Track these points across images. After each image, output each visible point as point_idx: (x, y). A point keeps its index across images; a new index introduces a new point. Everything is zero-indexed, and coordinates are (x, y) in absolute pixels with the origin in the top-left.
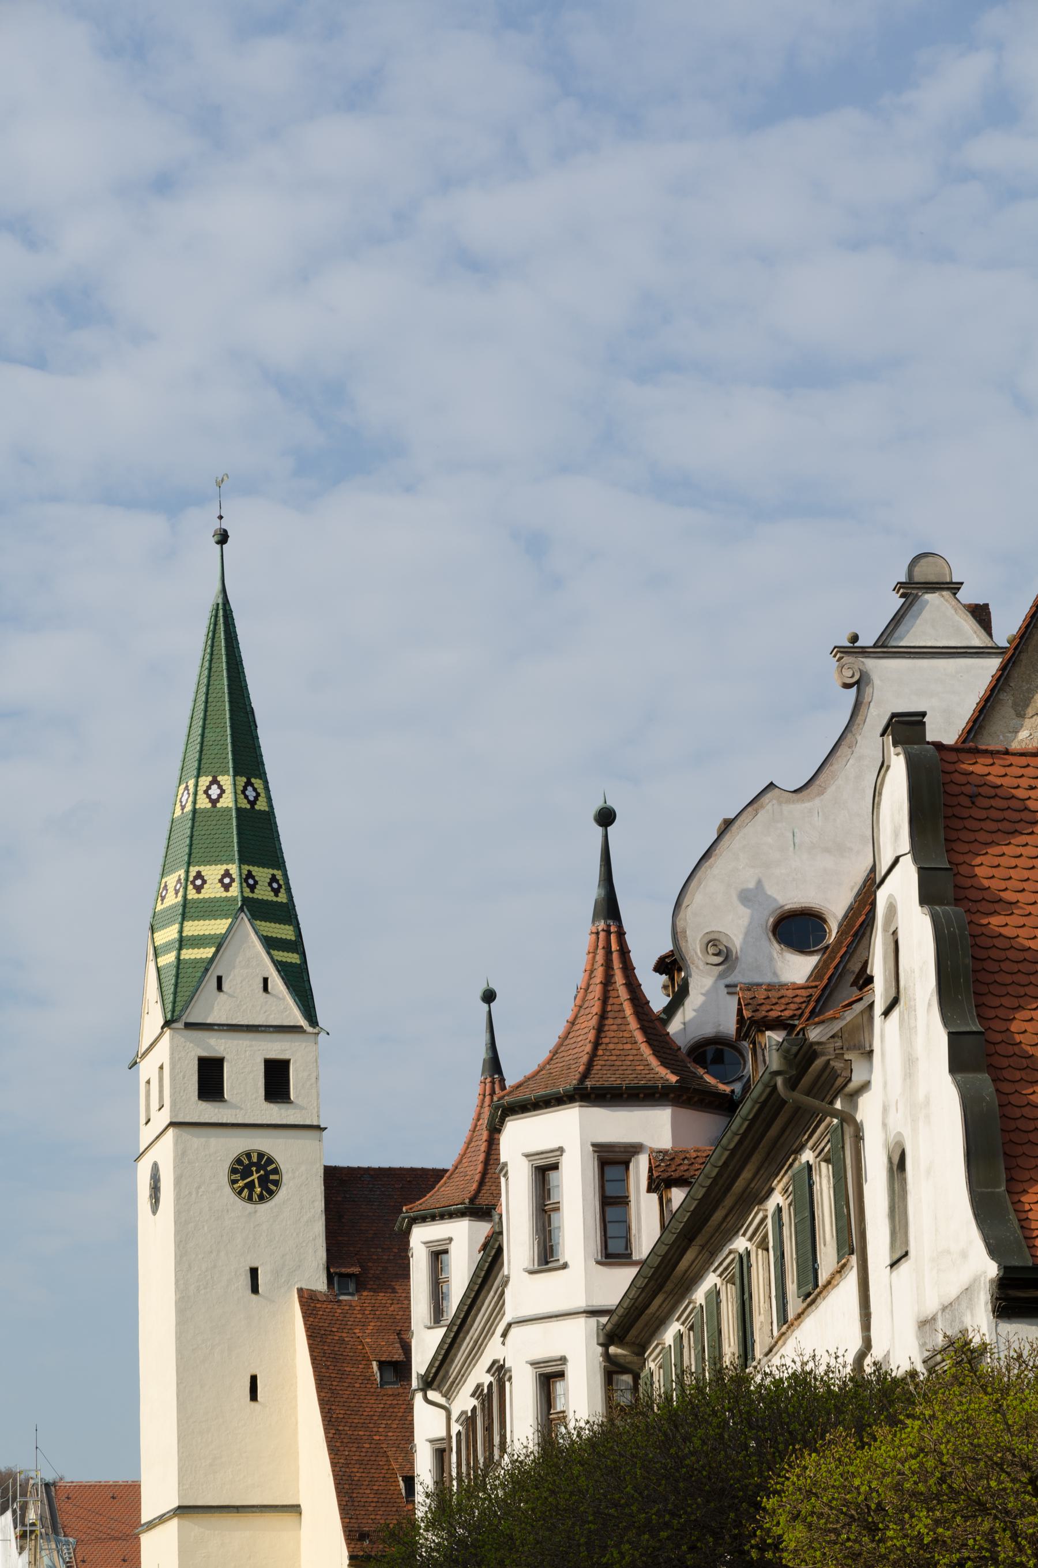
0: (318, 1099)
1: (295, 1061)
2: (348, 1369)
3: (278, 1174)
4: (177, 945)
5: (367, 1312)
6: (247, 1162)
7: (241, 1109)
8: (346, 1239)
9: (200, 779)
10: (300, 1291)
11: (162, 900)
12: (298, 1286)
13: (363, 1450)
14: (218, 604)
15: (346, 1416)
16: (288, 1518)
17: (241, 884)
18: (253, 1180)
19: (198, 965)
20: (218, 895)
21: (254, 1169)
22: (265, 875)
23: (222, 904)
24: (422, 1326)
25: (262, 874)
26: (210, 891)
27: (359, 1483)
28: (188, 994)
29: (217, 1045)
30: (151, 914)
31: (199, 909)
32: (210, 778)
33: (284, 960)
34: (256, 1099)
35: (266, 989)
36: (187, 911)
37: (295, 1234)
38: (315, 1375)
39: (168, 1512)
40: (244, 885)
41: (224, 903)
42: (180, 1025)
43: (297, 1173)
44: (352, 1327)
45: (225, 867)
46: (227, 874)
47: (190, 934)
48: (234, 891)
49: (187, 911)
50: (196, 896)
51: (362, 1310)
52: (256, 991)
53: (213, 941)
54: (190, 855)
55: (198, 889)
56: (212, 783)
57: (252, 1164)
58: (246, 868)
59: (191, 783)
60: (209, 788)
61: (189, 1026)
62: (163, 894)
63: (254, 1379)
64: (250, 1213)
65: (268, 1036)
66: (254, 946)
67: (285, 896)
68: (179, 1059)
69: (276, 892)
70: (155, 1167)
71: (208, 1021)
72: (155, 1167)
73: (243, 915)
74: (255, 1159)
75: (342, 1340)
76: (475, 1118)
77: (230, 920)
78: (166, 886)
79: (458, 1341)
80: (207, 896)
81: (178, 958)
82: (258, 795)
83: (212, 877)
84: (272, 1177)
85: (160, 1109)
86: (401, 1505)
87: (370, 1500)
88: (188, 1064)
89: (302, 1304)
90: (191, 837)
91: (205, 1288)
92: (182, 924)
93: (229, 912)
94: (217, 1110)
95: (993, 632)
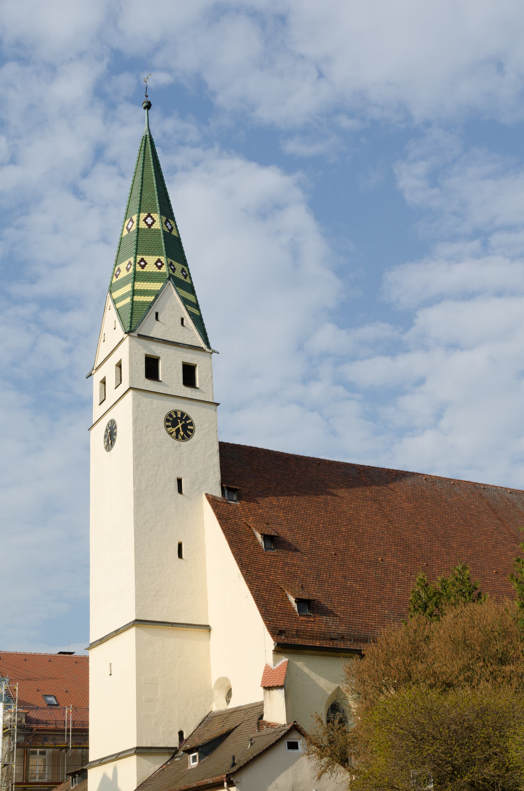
0: (212, 389)
1: (199, 367)
4: (131, 293)
6: (175, 417)
7: (170, 387)
9: (140, 214)
10: (207, 495)
14: (146, 135)
16: (202, 633)
18: (179, 428)
19: (145, 304)
20: (155, 271)
21: (179, 421)
23: (157, 275)
25: (178, 266)
26: (149, 268)
29: (156, 350)
30: (109, 284)
31: (143, 277)
32: (147, 214)
34: (178, 383)
36: (136, 277)
37: (203, 462)
38: (227, 539)
41: (158, 275)
42: (135, 334)
43: (203, 427)
46: (159, 261)
47: (139, 288)
48: (164, 269)
50: (141, 270)
52: (178, 324)
54: (137, 249)
55: (143, 267)
57: (177, 418)
58: (170, 260)
59: (135, 218)
61: (140, 336)
62: (117, 274)
63: (180, 546)
64: (177, 446)
65: (185, 350)
66: (176, 300)
68: (134, 353)
71: (151, 335)
73: (169, 282)
74: (179, 416)
75: (236, 523)
77: (162, 284)
81: (132, 300)
83: (151, 262)
84: (189, 427)
90: (137, 241)
91: (151, 486)
92: (134, 283)
94: (156, 386)
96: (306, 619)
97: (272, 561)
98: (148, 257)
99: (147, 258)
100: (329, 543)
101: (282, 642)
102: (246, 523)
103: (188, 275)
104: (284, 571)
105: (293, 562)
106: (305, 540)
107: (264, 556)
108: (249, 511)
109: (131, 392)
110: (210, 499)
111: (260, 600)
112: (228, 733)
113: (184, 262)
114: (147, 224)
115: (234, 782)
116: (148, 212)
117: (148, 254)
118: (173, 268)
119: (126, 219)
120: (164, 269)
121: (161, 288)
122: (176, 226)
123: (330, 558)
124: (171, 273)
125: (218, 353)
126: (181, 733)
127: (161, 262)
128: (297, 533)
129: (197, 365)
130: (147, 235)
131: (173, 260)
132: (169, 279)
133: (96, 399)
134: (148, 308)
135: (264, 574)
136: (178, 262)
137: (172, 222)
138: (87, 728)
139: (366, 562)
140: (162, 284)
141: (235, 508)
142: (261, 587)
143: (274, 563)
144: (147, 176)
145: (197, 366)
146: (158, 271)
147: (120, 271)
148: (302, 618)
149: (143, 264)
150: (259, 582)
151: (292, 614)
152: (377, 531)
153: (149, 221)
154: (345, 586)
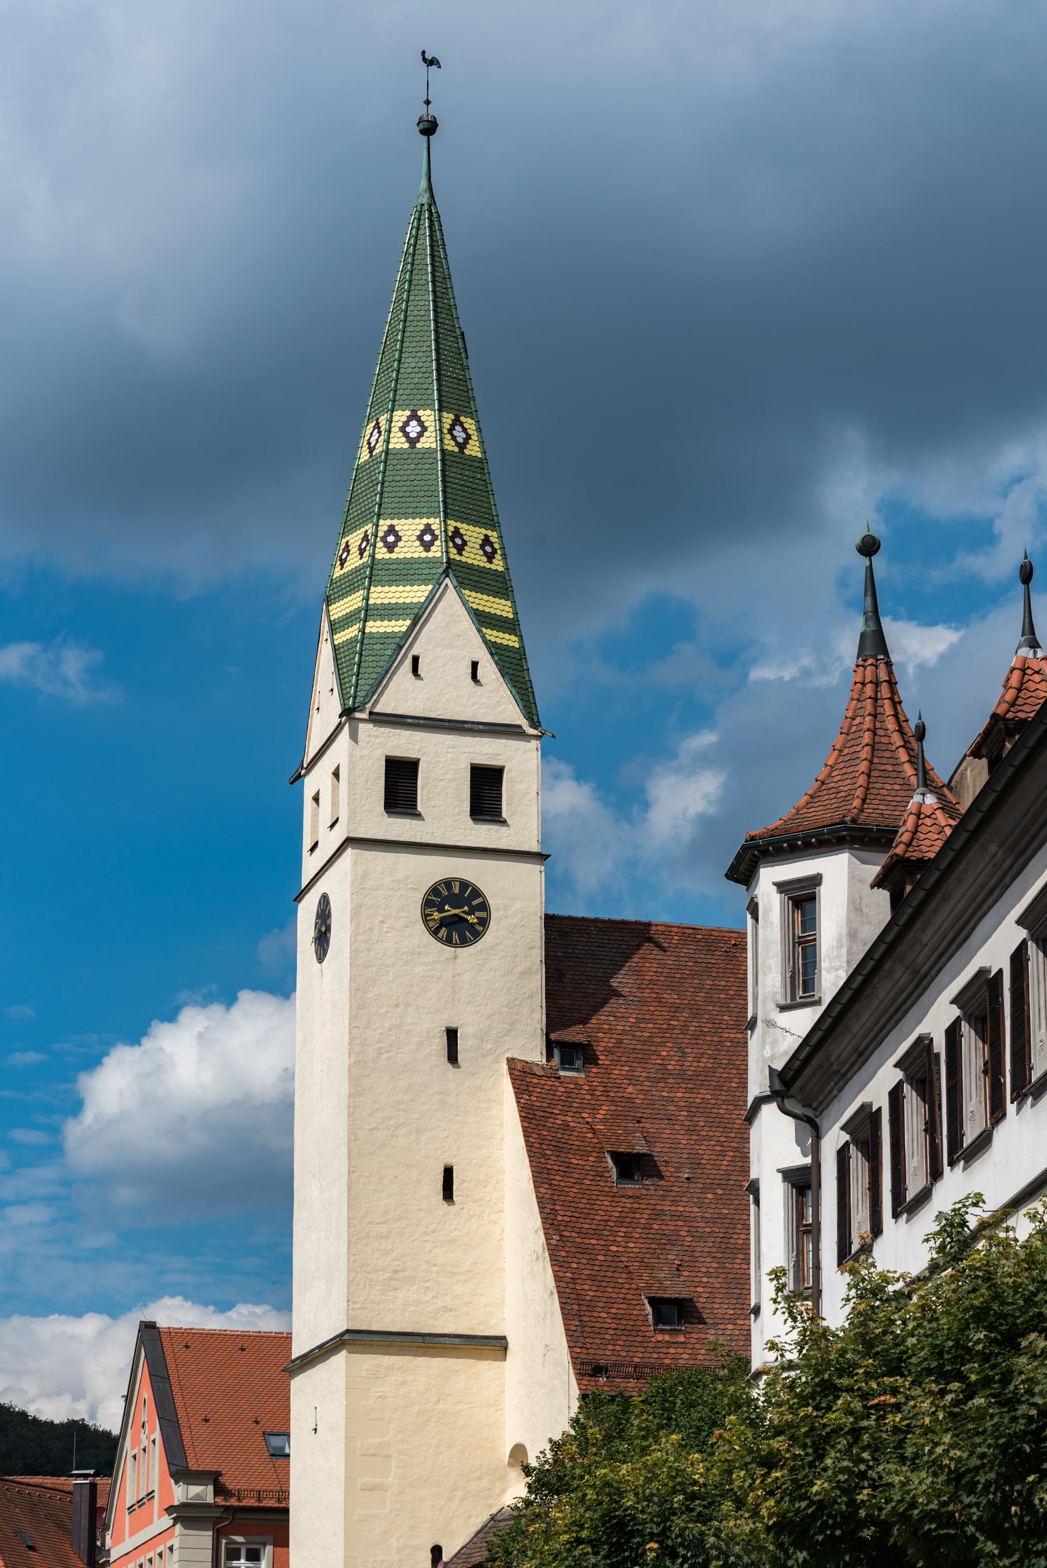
2: (574, 1161)
3: (487, 911)
5: (598, 1093)
6: (446, 894)
8: (568, 1002)
10: (511, 1061)
11: (342, 565)
12: (509, 1055)
13: (597, 1262)
15: (573, 1219)
17: (446, 541)
20: (416, 555)
22: (476, 535)
24: (772, 1005)
25: (473, 534)
26: (405, 549)
27: (592, 1304)
28: (374, 676)
32: (408, 413)
33: (499, 641)
34: (458, 814)
35: (474, 676)
39: (331, 1340)
40: (451, 544)
41: (424, 566)
44: (579, 1110)
45: (425, 521)
46: (428, 529)
47: (379, 601)
48: (437, 551)
50: (387, 556)
51: (592, 1091)
53: (408, 611)
58: (452, 524)
60: (406, 424)
62: (344, 557)
63: (448, 1172)
67: (501, 563)
69: (490, 557)
70: (325, 900)
72: (325, 900)
75: (566, 1125)
76: (683, 925)
77: (430, 587)
78: (347, 546)
79: (875, 981)
80: (401, 556)
82: (469, 437)
83: (409, 533)
85: (332, 826)
86: (647, 1334)
87: (608, 1326)
88: (373, 764)
89: (514, 1079)
93: (430, 577)
96: (667, 1338)
98: (403, 521)
102: (588, 1123)
103: (499, 551)
109: (349, 852)
116: (412, 408)
117: (406, 516)
120: (437, 551)
121: (427, 597)
126: (437, 1552)
127: (432, 532)
128: (708, 1138)
130: (406, 467)
132: (446, 574)
133: (307, 845)
134: (395, 650)
140: (430, 587)
141: (573, 1086)
144: (416, 313)
147: (348, 552)
148: (660, 1337)
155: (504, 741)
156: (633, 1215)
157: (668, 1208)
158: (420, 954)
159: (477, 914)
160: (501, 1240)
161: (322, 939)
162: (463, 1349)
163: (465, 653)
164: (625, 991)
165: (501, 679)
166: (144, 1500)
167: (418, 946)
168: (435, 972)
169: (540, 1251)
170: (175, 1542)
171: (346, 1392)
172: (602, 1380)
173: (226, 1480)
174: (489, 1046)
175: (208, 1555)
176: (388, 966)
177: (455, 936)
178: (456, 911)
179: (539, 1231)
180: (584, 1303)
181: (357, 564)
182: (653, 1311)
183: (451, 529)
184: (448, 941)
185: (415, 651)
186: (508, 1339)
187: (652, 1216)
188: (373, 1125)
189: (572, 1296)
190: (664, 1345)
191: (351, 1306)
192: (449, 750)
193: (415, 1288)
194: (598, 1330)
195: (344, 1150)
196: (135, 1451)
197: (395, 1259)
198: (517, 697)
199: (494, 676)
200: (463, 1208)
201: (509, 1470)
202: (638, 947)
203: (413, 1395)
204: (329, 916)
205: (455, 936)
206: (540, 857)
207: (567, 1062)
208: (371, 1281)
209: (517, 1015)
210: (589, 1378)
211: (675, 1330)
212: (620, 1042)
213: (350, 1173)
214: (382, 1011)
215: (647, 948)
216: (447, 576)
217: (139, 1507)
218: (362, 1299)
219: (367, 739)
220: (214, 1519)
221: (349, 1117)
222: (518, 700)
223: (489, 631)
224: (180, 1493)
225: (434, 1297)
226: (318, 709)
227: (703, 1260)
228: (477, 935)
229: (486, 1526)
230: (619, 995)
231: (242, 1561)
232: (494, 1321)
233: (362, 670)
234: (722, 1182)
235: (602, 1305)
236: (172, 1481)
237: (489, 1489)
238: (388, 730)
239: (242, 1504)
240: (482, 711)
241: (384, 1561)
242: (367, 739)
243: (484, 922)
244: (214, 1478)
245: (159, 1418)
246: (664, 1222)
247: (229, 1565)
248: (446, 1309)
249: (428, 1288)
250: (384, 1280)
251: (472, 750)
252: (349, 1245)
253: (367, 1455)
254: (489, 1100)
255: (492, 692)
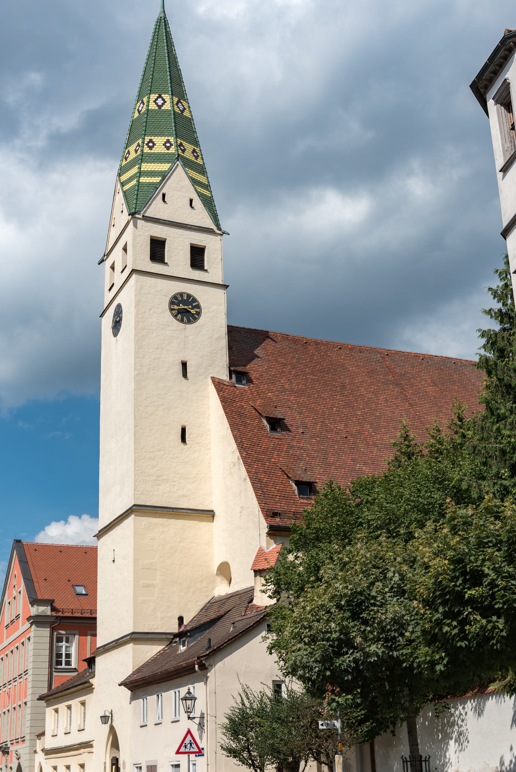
4: (138, 175)
6: (181, 299)
10: (213, 378)
20: (163, 151)
25: (189, 147)
26: (158, 149)
34: (185, 265)
40: (179, 148)
46: (168, 141)
47: (146, 169)
48: (172, 150)
49: (142, 158)
56: (158, 98)
58: (179, 141)
63: (183, 430)
69: (197, 157)
70: (119, 306)
77: (170, 164)
78: (129, 151)
81: (138, 181)
89: (215, 386)
95: (124, 245)
96: (306, 501)
97: (277, 444)
98: (156, 138)
99: (155, 139)
100: (341, 426)
101: (275, 524)
104: (288, 454)
105: (299, 445)
106: (316, 423)
107: (268, 439)
108: (258, 395)
109: (134, 276)
110: (215, 383)
111: (257, 482)
112: (219, 618)
113: (195, 142)
114: (158, 105)
115: (207, 665)
116: (159, 93)
118: (195, 154)
119: (138, 101)
120: (172, 150)
121: (169, 169)
122: (189, 107)
123: (340, 441)
124: (180, 153)
125: (228, 234)
126: (181, 619)
128: (308, 416)
129: (206, 246)
131: (184, 140)
132: (178, 159)
135: (266, 457)
136: (189, 143)
137: (184, 103)
138: (93, 616)
139: (379, 445)
140: (170, 164)
142: (261, 469)
143: (278, 446)
145: (206, 248)
146: (167, 151)
148: (302, 501)
149: (151, 145)
150: (259, 464)
151: (291, 496)
152: (396, 414)
153: (160, 102)
154: (353, 469)
155: (206, 235)
156: (280, 447)
157: (296, 444)
158: (168, 326)
159: (195, 309)
160: (210, 463)
161: (117, 325)
162: (192, 516)
163: (187, 195)
164: (261, 356)
165: (204, 208)
166: (14, 620)
167: (168, 322)
168: (176, 334)
169: (236, 460)
170: (32, 635)
171: (134, 536)
172: (278, 520)
173: (56, 605)
174: (202, 371)
175: (48, 640)
176: (153, 330)
177: (185, 319)
178: (186, 307)
179: (235, 452)
180: (263, 483)
181: (134, 157)
182: (298, 488)
183: (179, 142)
184: (182, 321)
185: (164, 191)
186: (215, 511)
187: (289, 448)
188: (147, 405)
189: (257, 480)
190: (305, 505)
191: (136, 493)
192: (180, 236)
193: (168, 485)
194: (272, 496)
195: (132, 416)
196: (10, 600)
197: (158, 470)
198: (211, 216)
199: (200, 206)
200: (191, 447)
201: (217, 577)
202: (264, 340)
203: (168, 538)
204: (121, 312)
205: (185, 319)
206: (225, 287)
207: (239, 381)
208: (146, 480)
209: (215, 357)
210: (271, 518)
211: (309, 498)
212: (262, 375)
213: (135, 427)
214: (151, 351)
215: (268, 341)
216: (178, 160)
217: (11, 624)
218: (141, 489)
219: (142, 227)
220: (51, 623)
221: (135, 400)
222: (212, 217)
223: (197, 187)
224: (35, 610)
225: (177, 490)
226: (114, 225)
227: (316, 468)
228: (195, 319)
229: (206, 606)
230: (259, 357)
231: (64, 643)
232: (207, 503)
233: (138, 197)
234: (318, 435)
235: (272, 485)
236: (30, 605)
237: (207, 587)
238: (151, 224)
239: (64, 615)
240: (195, 221)
241: (154, 624)
242: (142, 227)
243: (199, 314)
244: (50, 603)
245: (24, 578)
246: (295, 450)
247: (57, 645)
248: (183, 496)
249: (174, 485)
250: (153, 480)
251: (191, 237)
252: (135, 462)
253: (145, 569)
254: (203, 396)
255: (200, 213)
